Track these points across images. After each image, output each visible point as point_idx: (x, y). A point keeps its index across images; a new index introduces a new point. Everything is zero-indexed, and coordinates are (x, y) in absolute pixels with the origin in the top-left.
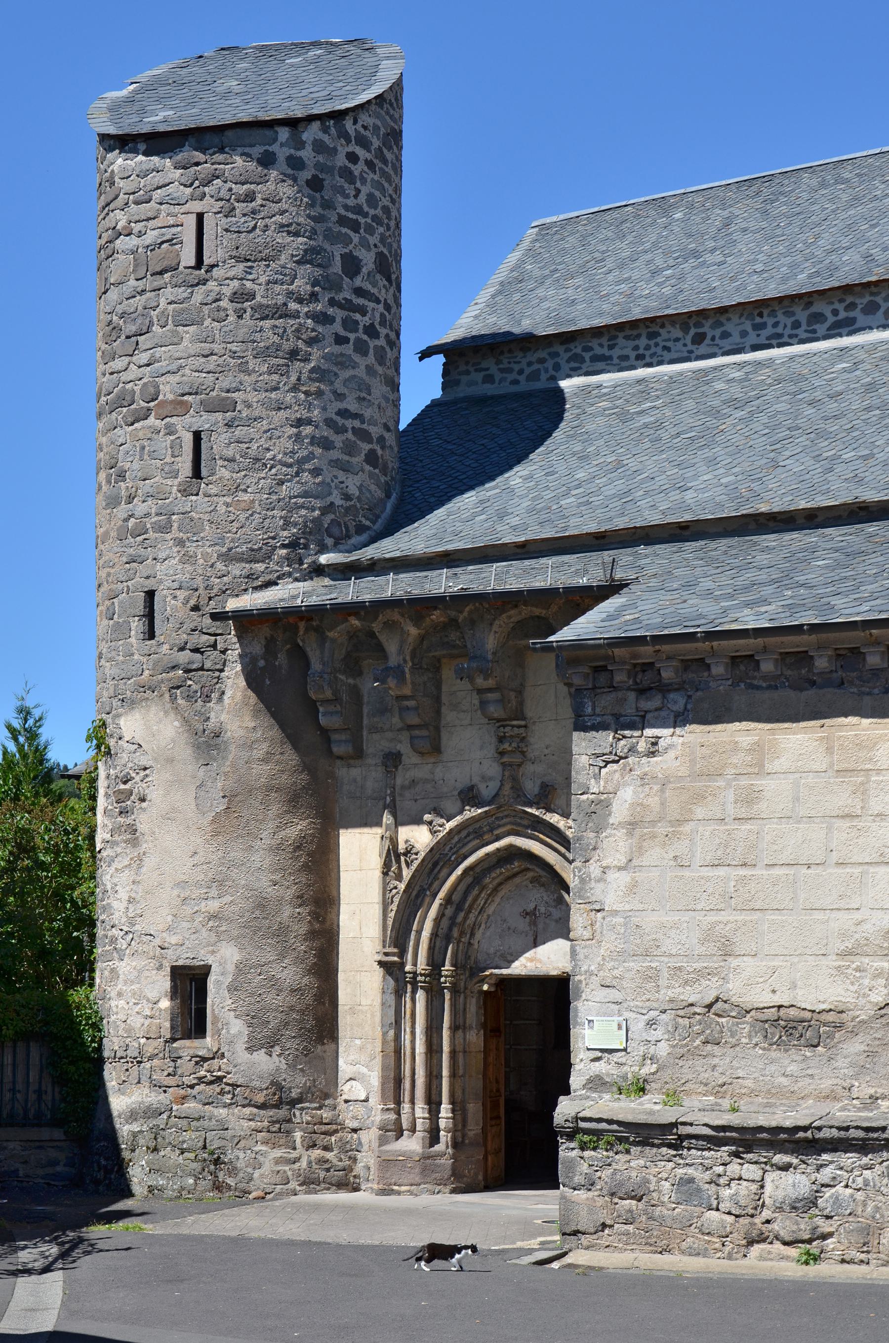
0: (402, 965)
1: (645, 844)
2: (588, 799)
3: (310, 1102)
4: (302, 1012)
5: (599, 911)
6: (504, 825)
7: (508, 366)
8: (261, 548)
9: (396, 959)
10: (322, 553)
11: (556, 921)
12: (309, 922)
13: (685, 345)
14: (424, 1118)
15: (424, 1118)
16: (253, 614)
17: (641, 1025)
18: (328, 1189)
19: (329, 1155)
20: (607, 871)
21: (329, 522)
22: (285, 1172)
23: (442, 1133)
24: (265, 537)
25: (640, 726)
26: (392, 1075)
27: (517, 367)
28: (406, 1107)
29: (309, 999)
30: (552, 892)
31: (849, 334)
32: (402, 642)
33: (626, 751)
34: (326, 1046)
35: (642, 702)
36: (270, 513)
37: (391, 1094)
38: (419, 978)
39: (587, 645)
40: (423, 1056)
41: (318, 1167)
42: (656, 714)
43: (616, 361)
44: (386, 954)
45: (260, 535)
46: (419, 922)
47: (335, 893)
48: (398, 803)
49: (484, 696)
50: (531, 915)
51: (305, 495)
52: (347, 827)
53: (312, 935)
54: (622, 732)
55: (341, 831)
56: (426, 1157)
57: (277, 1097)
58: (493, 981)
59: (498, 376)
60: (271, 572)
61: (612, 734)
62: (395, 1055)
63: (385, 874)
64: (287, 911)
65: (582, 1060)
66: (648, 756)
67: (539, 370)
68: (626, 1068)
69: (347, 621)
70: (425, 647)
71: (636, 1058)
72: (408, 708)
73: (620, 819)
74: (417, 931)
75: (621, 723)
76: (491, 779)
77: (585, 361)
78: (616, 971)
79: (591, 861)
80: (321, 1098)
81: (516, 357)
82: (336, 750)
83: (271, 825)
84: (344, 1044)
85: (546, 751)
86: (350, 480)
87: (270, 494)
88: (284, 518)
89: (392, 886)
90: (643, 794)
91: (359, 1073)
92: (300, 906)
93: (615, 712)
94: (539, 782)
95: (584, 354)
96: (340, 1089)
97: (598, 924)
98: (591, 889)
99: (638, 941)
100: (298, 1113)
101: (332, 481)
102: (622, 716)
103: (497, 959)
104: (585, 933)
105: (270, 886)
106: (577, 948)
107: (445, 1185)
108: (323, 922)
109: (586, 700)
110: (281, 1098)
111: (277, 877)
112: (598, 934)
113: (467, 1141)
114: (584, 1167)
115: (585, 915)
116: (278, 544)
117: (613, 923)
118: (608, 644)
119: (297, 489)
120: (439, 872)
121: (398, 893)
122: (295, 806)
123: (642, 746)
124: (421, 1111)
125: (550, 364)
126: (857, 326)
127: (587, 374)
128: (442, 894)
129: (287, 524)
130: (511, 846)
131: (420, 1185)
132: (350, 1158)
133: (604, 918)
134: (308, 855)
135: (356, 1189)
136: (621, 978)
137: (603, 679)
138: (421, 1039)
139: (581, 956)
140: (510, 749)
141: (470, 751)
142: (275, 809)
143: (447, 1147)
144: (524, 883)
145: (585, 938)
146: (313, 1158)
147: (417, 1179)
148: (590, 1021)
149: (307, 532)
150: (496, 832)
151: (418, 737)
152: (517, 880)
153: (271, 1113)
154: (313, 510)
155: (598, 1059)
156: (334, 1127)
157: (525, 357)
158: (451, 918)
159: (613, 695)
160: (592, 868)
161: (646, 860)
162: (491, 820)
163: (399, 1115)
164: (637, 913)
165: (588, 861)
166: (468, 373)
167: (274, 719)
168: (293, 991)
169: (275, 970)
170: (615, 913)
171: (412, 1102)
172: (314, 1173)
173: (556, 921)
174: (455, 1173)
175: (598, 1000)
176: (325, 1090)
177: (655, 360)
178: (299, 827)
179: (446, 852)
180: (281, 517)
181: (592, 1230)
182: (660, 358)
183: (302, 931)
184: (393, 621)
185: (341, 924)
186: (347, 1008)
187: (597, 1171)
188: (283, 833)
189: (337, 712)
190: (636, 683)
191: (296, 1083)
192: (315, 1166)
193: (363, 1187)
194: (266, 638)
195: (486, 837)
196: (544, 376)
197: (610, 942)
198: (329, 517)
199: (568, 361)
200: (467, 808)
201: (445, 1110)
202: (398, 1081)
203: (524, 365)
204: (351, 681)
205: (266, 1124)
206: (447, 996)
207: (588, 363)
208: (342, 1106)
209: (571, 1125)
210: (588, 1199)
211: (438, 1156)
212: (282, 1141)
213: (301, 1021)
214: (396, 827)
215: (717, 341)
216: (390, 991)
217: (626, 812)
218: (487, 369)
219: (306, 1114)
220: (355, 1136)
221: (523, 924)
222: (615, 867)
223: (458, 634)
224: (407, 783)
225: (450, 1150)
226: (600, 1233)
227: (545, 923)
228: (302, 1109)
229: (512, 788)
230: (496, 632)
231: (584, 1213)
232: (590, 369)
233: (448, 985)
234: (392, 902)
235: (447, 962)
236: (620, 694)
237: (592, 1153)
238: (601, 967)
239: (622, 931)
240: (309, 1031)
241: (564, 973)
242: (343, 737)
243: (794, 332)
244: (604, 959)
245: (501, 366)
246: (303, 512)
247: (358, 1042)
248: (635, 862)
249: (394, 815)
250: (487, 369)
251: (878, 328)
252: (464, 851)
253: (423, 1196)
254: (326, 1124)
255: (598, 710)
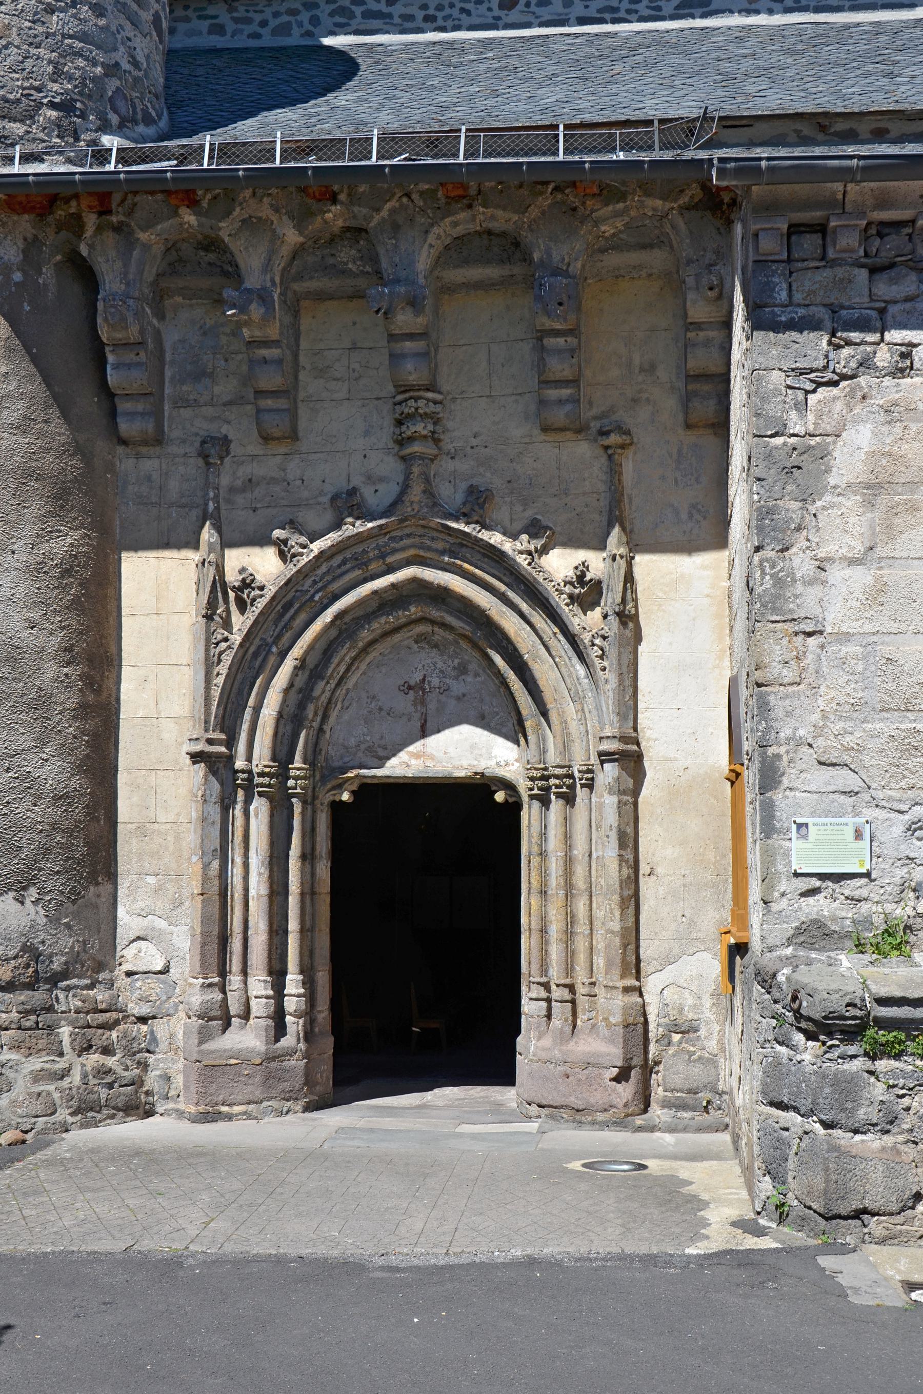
0: (231, 759)
1: (897, 521)
2: (785, 444)
3: (80, 977)
4: (69, 832)
5: (810, 634)
6: (403, 549)
7: (246, 14)
8: (18, 101)
9: (223, 749)
10: (106, 134)
11: (458, 699)
12: (81, 690)
13: (490, 9)
14: (267, 997)
15: (267, 997)
16: (28, 183)
17: (898, 830)
18: (113, 1117)
19: (111, 1062)
20: (827, 566)
21: (114, 89)
22: (49, 1094)
23: (289, 1019)
24: (26, 84)
25: (879, 324)
26: (216, 932)
27: (258, 18)
28: (235, 981)
29: (78, 812)
30: (450, 657)
31: (704, 16)
32: (272, 253)
33: (853, 364)
34: (101, 887)
35: (881, 286)
36: (33, 51)
37: (214, 960)
38: (257, 780)
39: (825, 168)
40: (265, 901)
41: (97, 1082)
42: (908, 306)
43: (397, 20)
44: (210, 742)
45: (18, 81)
46: (257, 694)
47: (113, 649)
48: (223, 512)
49: (399, 345)
50: (417, 690)
51: (83, 37)
52: (137, 546)
53: (83, 711)
54: (845, 335)
55: (124, 555)
56: (271, 1058)
57: (31, 970)
58: (354, 787)
59: (230, 27)
60: (34, 140)
61: (826, 338)
62: (220, 898)
63: (209, 618)
64: (51, 670)
65: (783, 895)
66: (893, 375)
67: (289, 23)
68: (864, 907)
69: (176, 214)
70: (293, 271)
71: (889, 889)
72: (265, 361)
73: (851, 478)
74: (254, 708)
75: (839, 321)
76: (381, 480)
77: (355, 17)
78: (848, 738)
79: (794, 550)
80: (93, 971)
81: (257, 4)
82: (125, 427)
83: (29, 531)
84: (127, 884)
85: (474, 442)
86: (138, 40)
87: (34, 22)
88: (55, 64)
89: (219, 637)
90: (892, 438)
91: (153, 928)
92: (68, 663)
93: (832, 300)
94: (463, 486)
95: (353, 8)
96: (118, 954)
97: (810, 657)
98: (796, 597)
99: (891, 686)
100: (61, 996)
101: (119, 33)
102: (842, 307)
103: (360, 754)
104: (785, 672)
105: (25, 628)
106: (772, 698)
107: (296, 1099)
108: (98, 692)
109: (776, 280)
110: (36, 971)
111: (36, 615)
112: (810, 677)
113: (317, 1030)
114: (878, 1090)
115: (785, 642)
116: (45, 101)
117: (842, 654)
118: (864, 169)
119: (72, 27)
120: (293, 618)
121: (229, 647)
122: (63, 507)
123: (883, 357)
124: (259, 985)
125: (305, 17)
126: (712, 7)
127: (357, 32)
128: (297, 651)
129: (58, 74)
130: (415, 580)
131: (261, 1102)
132: (139, 1063)
133: (822, 647)
134: (80, 584)
135: (149, 1113)
136: (860, 749)
137: (809, 243)
138: (260, 874)
139: (779, 712)
140: (424, 432)
141: (347, 438)
142: (35, 507)
143: (299, 1040)
144: (406, 643)
145: (785, 681)
146: (88, 1068)
147: (258, 1094)
148: (800, 826)
149: (91, 90)
150: (390, 560)
151: (270, 411)
152: (397, 637)
153: (22, 998)
154: (95, 65)
155: (813, 892)
156: (114, 1015)
157: (269, 5)
158: (300, 691)
159: (827, 273)
160: (796, 562)
161: (904, 546)
162: (382, 541)
163: (224, 992)
164: (887, 639)
165: (787, 549)
166: (187, 20)
167: (36, 366)
168: (57, 798)
169: (31, 764)
170: (846, 637)
171: (244, 972)
172: (91, 1092)
173: (458, 699)
174: (309, 1081)
175: (813, 788)
176: (100, 957)
177: (449, 23)
178: (69, 540)
179: (305, 588)
180: (50, 62)
181: (895, 1208)
182: (456, 22)
183: (71, 704)
184: (260, 219)
185: (122, 697)
186: (132, 827)
187: (903, 1096)
188: (46, 546)
189: (138, 364)
190: (866, 255)
191: (60, 946)
192: (93, 1081)
193: (160, 1109)
194: (25, 239)
195: (373, 566)
196: (296, 31)
197: (836, 687)
198: (113, 84)
199: (331, 14)
200: (350, 520)
201: (293, 983)
202: (224, 940)
203: (268, 13)
204: (155, 321)
205: (14, 1015)
206: (297, 808)
207: (359, 18)
208: (122, 982)
209: (859, 1013)
210: (883, 1149)
211: (287, 1054)
212: (42, 1043)
213: (68, 847)
214: (222, 549)
215: (533, 8)
216: (213, 800)
217: (860, 466)
218: (215, 17)
219: (74, 996)
220: (144, 1028)
221: (404, 703)
222: (843, 558)
223: (353, 252)
224: (239, 483)
225: (302, 1046)
226: (909, 1212)
227: (439, 701)
228: (68, 989)
229: (424, 492)
230: (431, 246)
231: (877, 1174)
232: (362, 27)
233: (299, 790)
234: (219, 661)
235: (298, 757)
236: (840, 272)
237: (893, 1063)
238: (819, 731)
239: (860, 668)
240: (79, 863)
241: (476, 773)
242: (140, 407)
243: (633, 7)
244: (825, 717)
245: (235, 15)
246: (81, 62)
247: (151, 880)
248: (879, 551)
249: (218, 528)
250: (215, 17)
251: (740, 12)
252: (336, 586)
253: (266, 1120)
254: (102, 1011)
255: (798, 297)
